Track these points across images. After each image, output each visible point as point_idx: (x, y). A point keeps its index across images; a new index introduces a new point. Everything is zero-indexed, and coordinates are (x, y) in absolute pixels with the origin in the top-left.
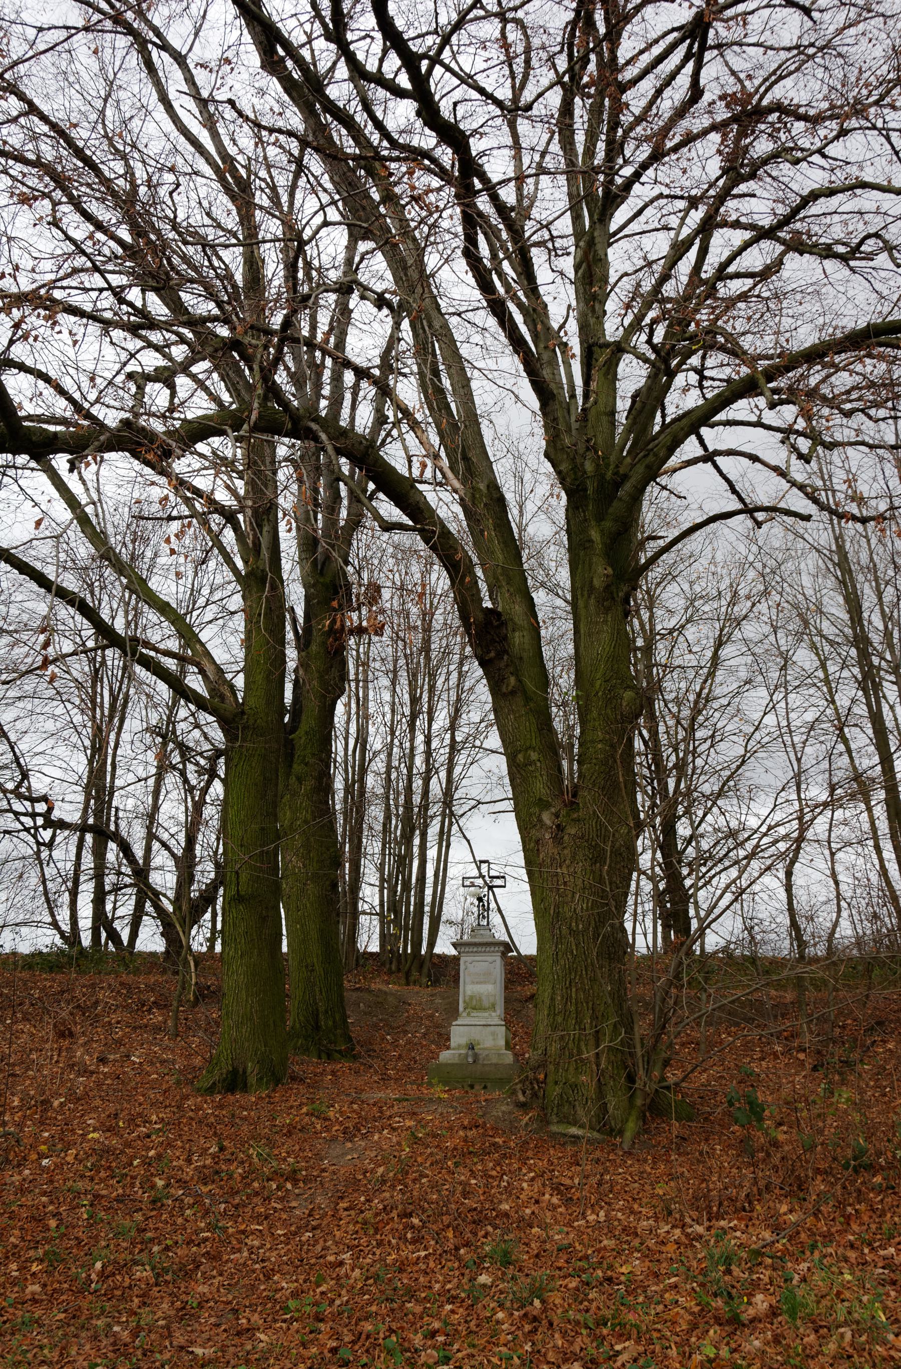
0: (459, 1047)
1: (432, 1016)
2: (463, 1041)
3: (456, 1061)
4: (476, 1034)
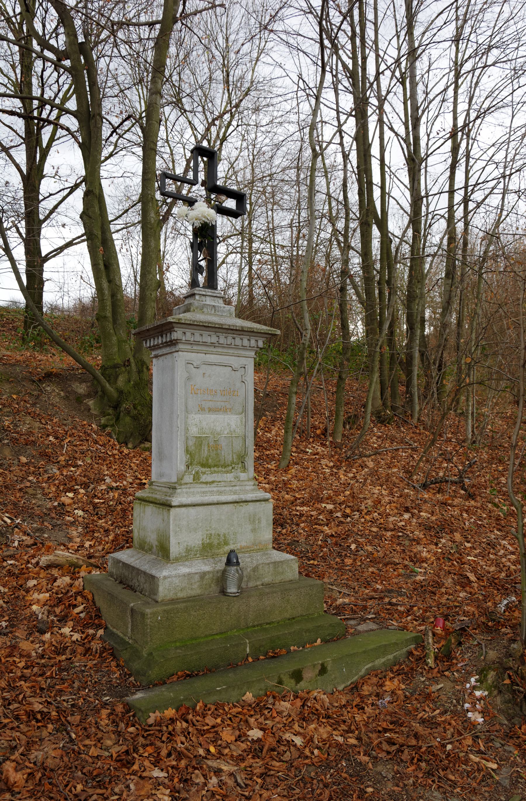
0: (188, 555)
2: (196, 540)
3: (196, 590)
4: (221, 521)
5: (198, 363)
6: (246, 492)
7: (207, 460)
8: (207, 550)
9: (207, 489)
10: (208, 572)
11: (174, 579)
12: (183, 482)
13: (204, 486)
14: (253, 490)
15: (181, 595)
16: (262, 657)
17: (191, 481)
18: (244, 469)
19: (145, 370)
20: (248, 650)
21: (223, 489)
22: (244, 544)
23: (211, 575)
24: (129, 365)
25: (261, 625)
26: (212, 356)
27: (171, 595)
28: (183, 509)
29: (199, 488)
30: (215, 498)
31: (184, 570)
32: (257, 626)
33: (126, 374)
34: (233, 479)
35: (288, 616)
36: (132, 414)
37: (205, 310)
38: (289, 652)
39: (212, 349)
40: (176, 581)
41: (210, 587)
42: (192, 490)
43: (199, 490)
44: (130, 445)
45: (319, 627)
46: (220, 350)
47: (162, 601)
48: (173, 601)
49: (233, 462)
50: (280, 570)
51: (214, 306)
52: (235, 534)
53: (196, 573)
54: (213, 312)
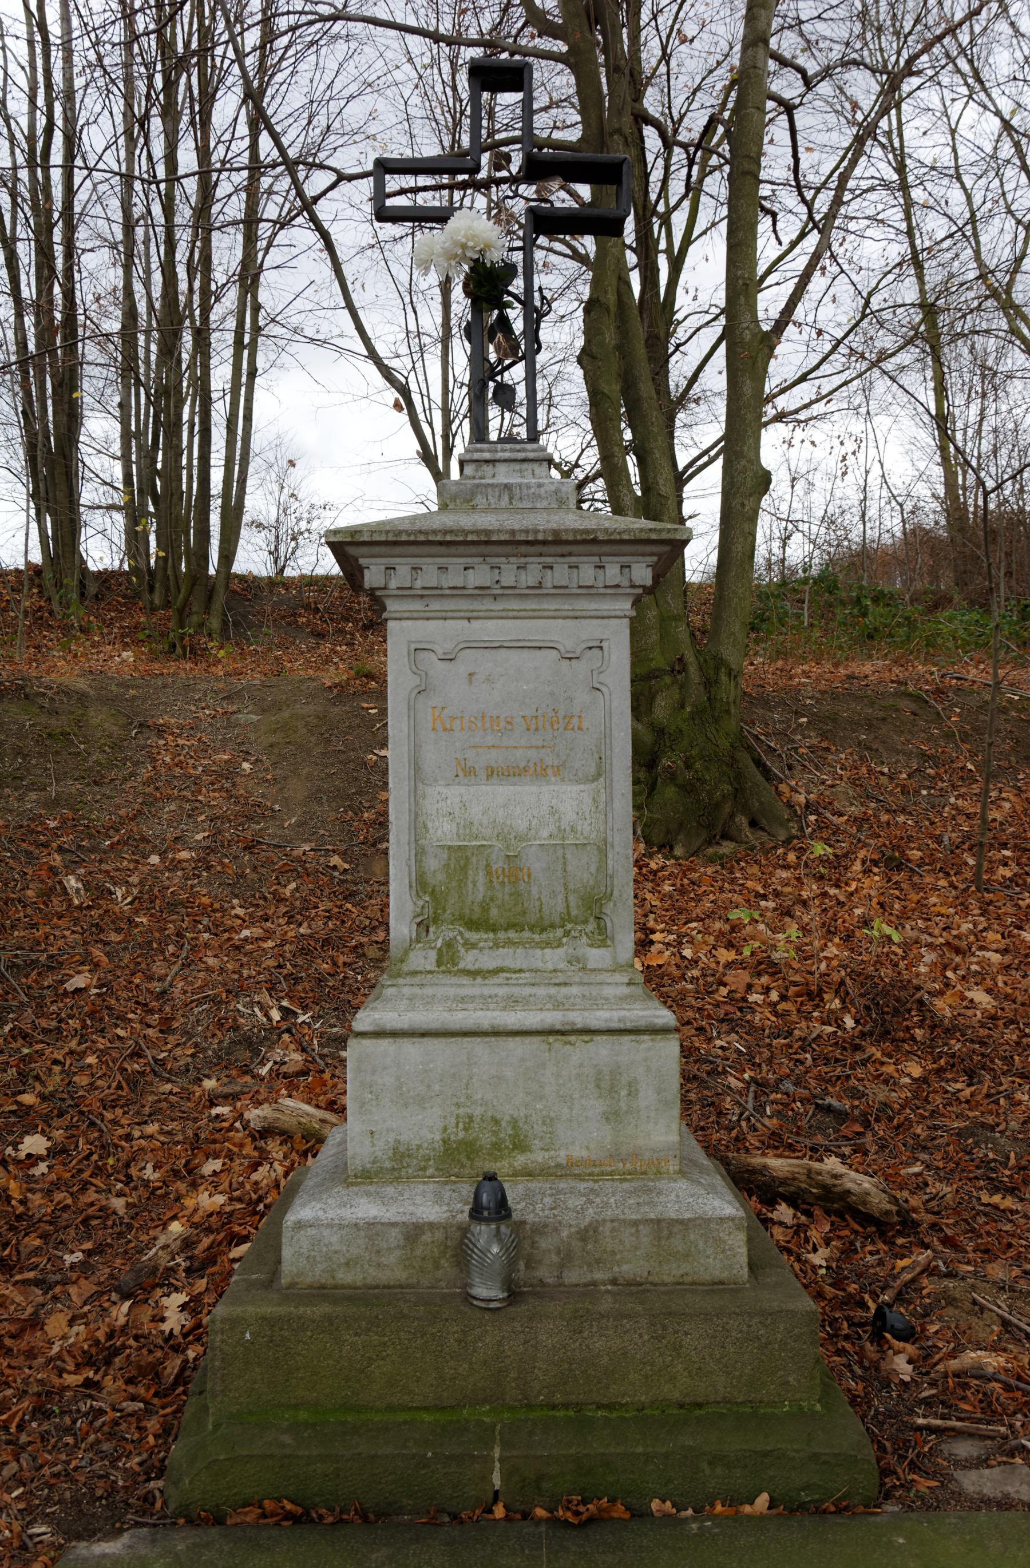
0: (397, 1168)
1: (230, 772)
2: (425, 1127)
3: (391, 1268)
4: (503, 1084)
5: (449, 646)
6: (596, 1003)
7: (485, 910)
8: (453, 1156)
9: (476, 991)
10: (431, 1225)
11: (326, 1232)
12: (405, 968)
13: (465, 980)
14: (623, 999)
15: (344, 1277)
16: (540, 1512)
17: (433, 967)
18: (603, 937)
19: (724, 678)
20: (497, 1480)
21: (528, 991)
22: (578, 1152)
23: (439, 1235)
24: (684, 669)
25: (579, 1406)
26: (491, 624)
27: (317, 1274)
28: (384, 1043)
29: (450, 987)
30: (485, 1018)
31: (366, 1209)
32: (566, 1406)
33: (676, 687)
34: (562, 966)
35: (677, 1395)
36: (680, 780)
37: (480, 500)
38: (640, 1514)
39: (488, 604)
40: (334, 1239)
41: (437, 1267)
42: (429, 991)
43: (451, 992)
44: (678, 851)
45: (766, 1454)
46: (515, 605)
47: (292, 1285)
48: (321, 1292)
49: (567, 917)
50: (678, 1244)
51: (507, 487)
52: (549, 1121)
53: (393, 1224)
54: (505, 501)
